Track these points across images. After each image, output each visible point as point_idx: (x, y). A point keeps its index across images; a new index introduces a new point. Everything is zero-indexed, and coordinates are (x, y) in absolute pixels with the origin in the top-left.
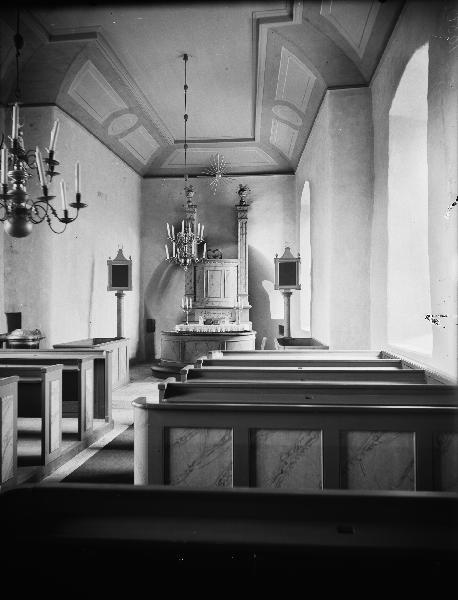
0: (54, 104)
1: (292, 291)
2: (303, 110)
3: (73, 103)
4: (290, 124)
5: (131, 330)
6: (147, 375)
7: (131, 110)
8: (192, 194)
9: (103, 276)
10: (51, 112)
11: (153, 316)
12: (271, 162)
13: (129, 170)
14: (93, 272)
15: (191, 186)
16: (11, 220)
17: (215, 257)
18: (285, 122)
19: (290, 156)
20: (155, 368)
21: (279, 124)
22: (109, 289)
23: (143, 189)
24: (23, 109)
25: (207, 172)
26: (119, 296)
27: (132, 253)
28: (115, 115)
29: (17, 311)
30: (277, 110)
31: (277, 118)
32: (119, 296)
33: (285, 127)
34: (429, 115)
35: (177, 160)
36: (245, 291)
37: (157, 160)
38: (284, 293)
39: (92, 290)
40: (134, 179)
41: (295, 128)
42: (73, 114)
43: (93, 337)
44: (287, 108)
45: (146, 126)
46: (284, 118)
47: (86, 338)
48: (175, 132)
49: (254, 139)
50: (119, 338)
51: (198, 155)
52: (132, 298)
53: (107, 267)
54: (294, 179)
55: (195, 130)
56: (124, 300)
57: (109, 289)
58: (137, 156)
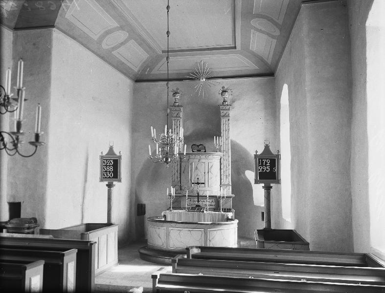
0: (53, 26)
1: (272, 185)
2: (280, 22)
3: (69, 24)
4: (268, 34)
5: (120, 212)
6: (136, 257)
7: (122, 28)
8: (178, 97)
9: (95, 169)
10: (50, 35)
11: (145, 200)
12: (250, 66)
13: (122, 77)
14: (87, 164)
15: (178, 89)
16: (270, 64)
17: (199, 151)
18: (260, 31)
19: (269, 61)
20: (143, 251)
21: (257, 33)
22: (101, 180)
23: (135, 91)
24: (20, 33)
25: (191, 77)
26: (110, 186)
27: (123, 150)
28: (108, 33)
29: (17, 201)
30: (255, 23)
31: (257, 30)
32: (110, 186)
33: (265, 37)
34: (118, 254)
35: (161, 69)
36: (228, 181)
37: (149, 65)
38: (263, 187)
39: (86, 181)
40: (126, 83)
41: (273, 37)
42: (71, 33)
43: (86, 221)
44: (264, 21)
45: (136, 40)
46: (263, 29)
47: (79, 223)
48: (160, 45)
49: (235, 48)
50: (109, 224)
51: (180, 63)
52: (121, 189)
53: (99, 161)
54: (275, 79)
55: (176, 42)
56: (114, 190)
57: (101, 180)
58: (129, 64)
